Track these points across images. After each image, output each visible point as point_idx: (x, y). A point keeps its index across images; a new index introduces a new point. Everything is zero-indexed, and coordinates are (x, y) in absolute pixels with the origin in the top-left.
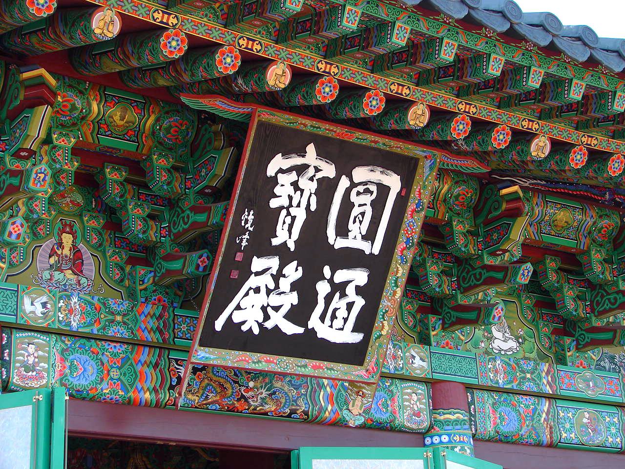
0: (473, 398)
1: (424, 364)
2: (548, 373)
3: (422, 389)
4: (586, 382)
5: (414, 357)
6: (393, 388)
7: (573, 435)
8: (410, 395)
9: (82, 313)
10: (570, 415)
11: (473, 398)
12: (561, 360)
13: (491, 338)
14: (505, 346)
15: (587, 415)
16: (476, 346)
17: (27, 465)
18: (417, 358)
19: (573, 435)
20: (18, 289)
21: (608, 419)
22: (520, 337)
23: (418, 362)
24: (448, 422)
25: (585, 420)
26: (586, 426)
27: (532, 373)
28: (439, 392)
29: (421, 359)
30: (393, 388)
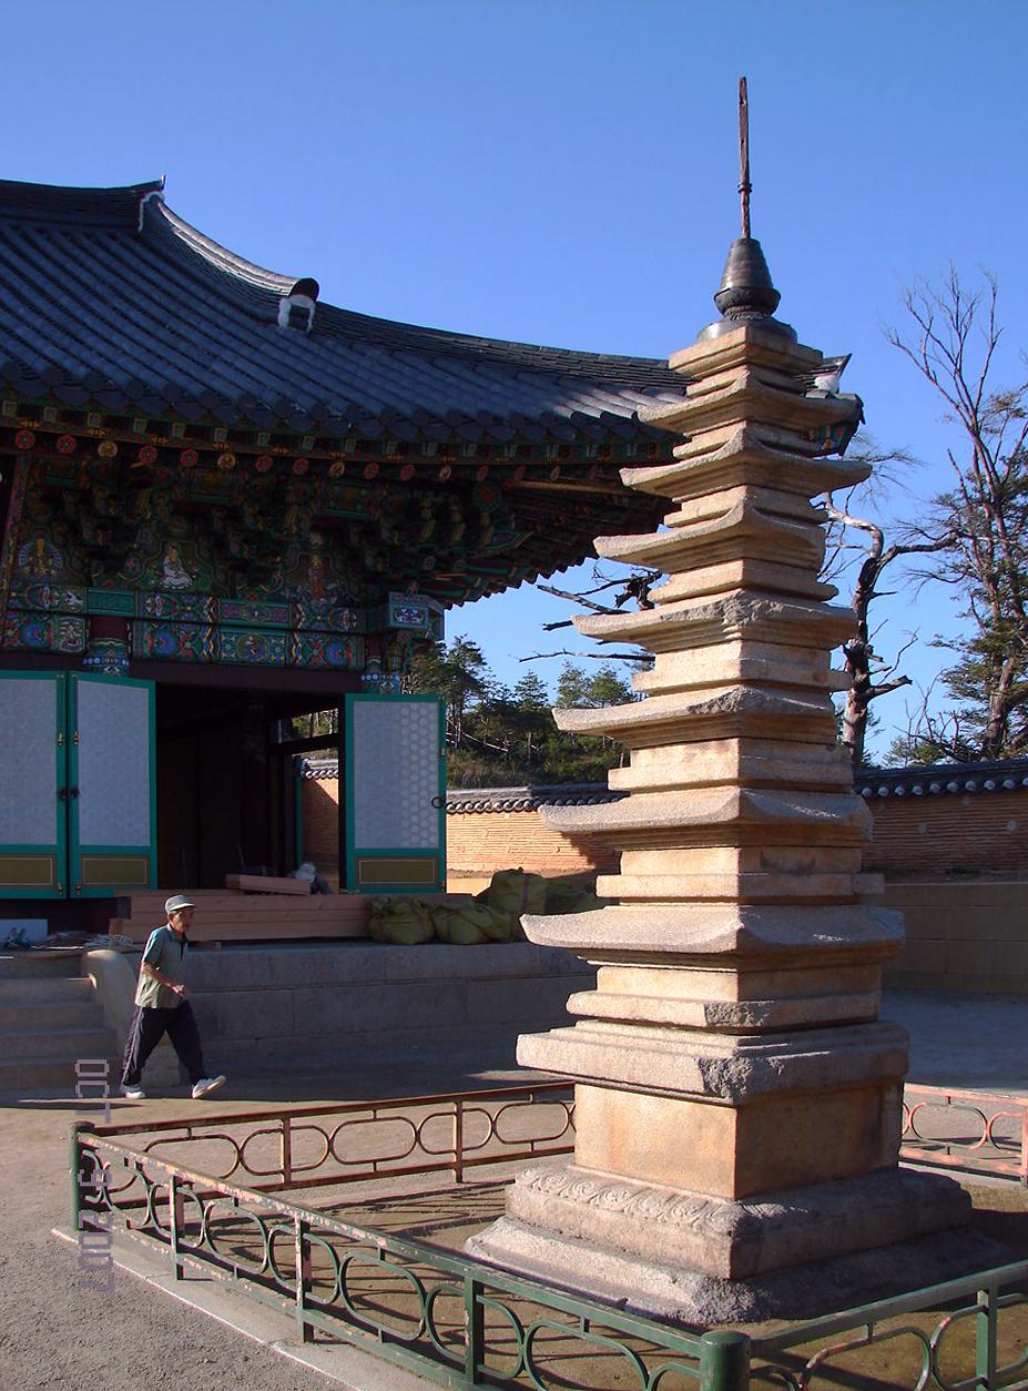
0: (131, 627)
1: (80, 602)
2: (300, 620)
3: (79, 621)
4: (252, 611)
5: (70, 597)
6: (50, 621)
7: (233, 656)
8: (67, 626)
9: (164, 605)
10: (233, 639)
11: (131, 627)
12: (234, 597)
13: (163, 575)
14: (176, 582)
15: (251, 638)
16: (146, 583)
17: (1024, 1307)
18: (74, 597)
19: (233, 656)
20: (380, 1120)
21: (273, 641)
22: (195, 573)
23: (74, 600)
24: (101, 647)
25: (248, 643)
26: (249, 647)
27: (316, 620)
28: (97, 626)
29: (78, 598)
30: (50, 621)
